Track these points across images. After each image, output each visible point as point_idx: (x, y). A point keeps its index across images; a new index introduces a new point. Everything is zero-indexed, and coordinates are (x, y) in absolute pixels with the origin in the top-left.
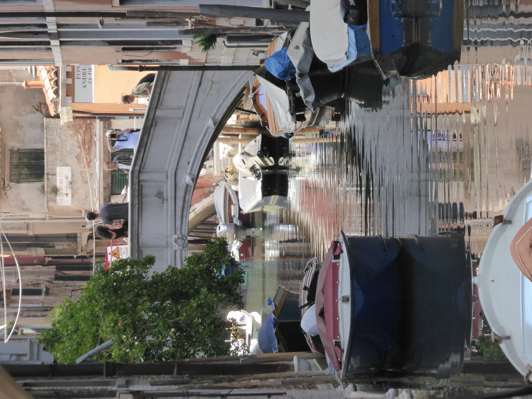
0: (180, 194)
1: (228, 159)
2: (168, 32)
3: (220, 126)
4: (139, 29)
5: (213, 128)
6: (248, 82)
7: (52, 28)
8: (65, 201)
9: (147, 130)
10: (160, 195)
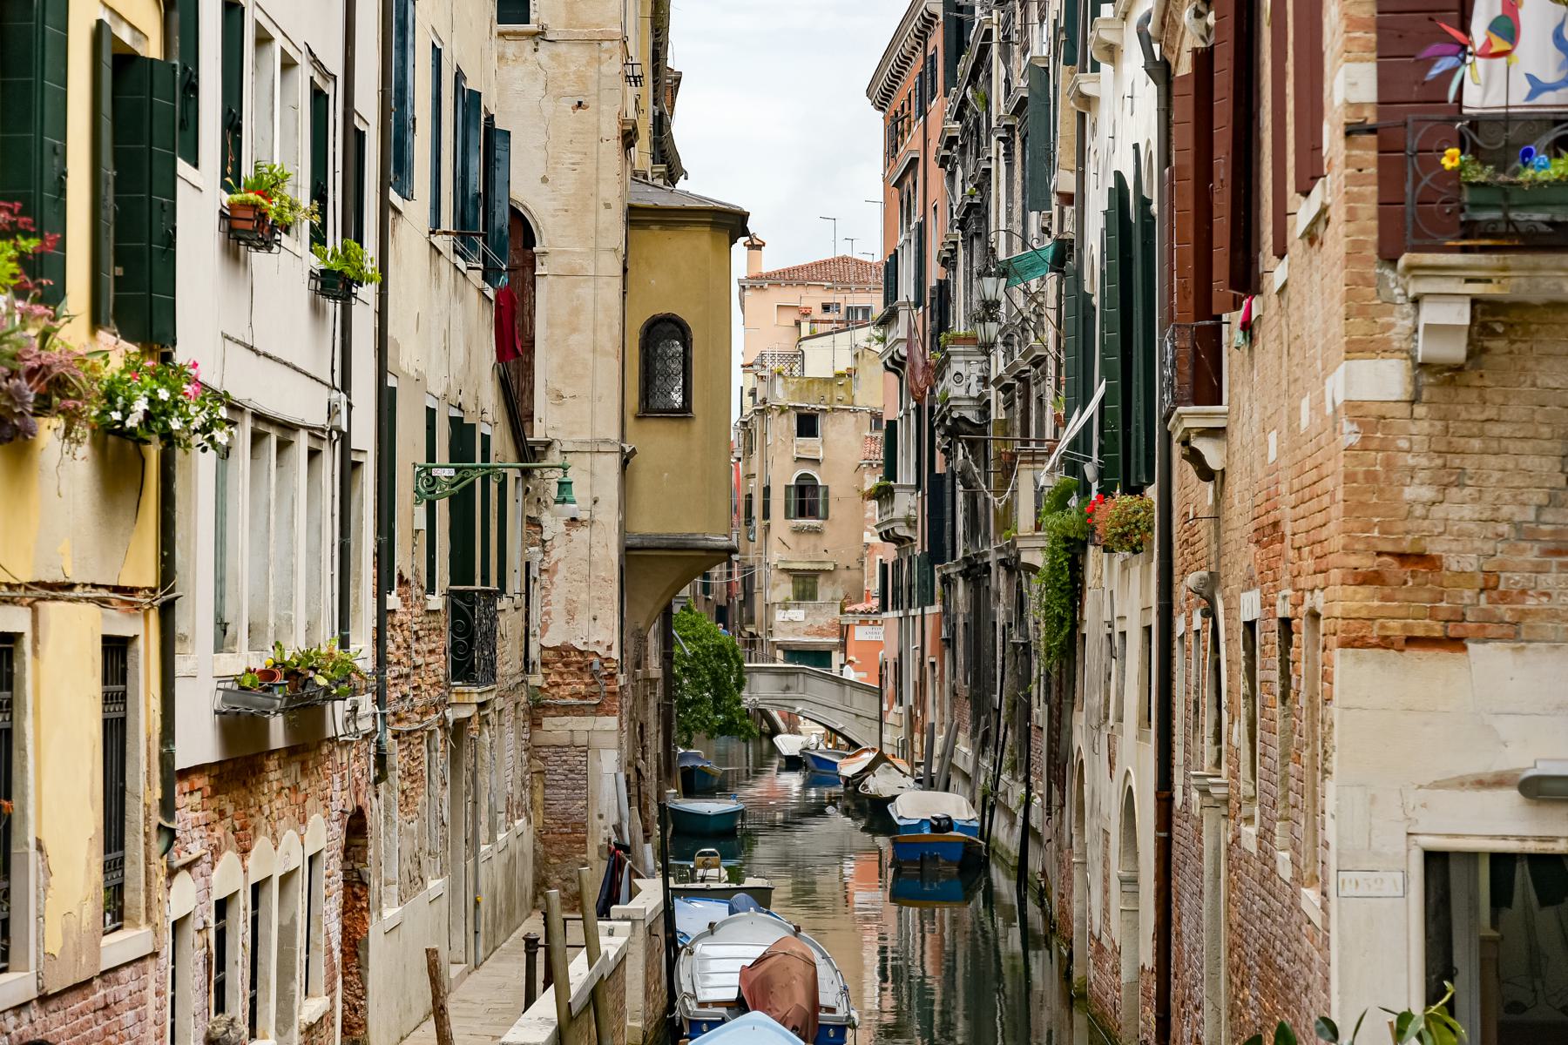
0: (788, 703)
1: (835, 783)
2: (909, 698)
3: (838, 733)
4: (911, 675)
5: (836, 727)
6: (196, 166)
7: (912, 612)
8: (780, 616)
9: (835, 679)
10: (788, 688)
